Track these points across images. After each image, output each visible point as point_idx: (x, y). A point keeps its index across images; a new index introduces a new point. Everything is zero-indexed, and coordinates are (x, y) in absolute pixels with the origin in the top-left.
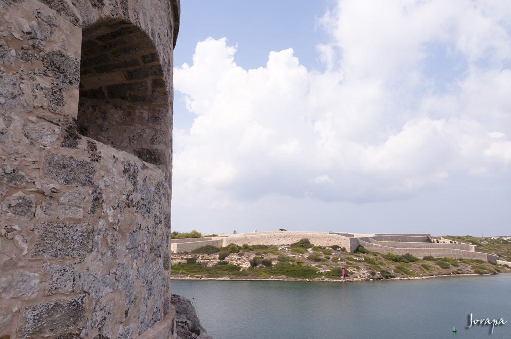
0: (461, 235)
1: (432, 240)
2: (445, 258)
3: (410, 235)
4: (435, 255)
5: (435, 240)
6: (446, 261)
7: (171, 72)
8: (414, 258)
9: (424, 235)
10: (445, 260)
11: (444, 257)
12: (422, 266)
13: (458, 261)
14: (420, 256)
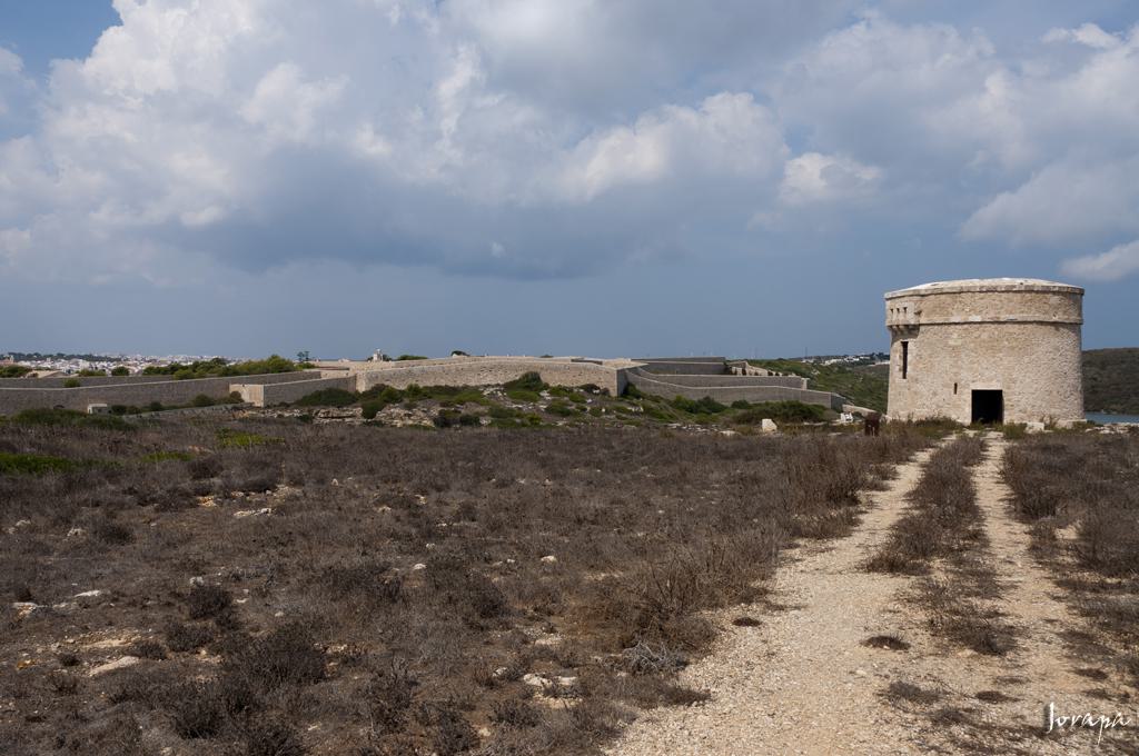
1: (734, 369)
5: (740, 370)
9: (714, 360)
14: (727, 402)
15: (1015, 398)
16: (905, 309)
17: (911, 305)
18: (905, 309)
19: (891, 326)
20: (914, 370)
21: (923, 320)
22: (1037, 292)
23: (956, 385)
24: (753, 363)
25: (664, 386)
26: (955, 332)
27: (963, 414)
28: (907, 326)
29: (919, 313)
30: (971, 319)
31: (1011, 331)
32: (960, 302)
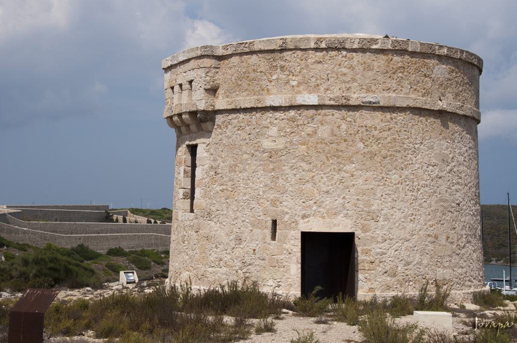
0: (154, 208)
1: (115, 217)
2: (143, 251)
3: (73, 207)
4: (126, 246)
5: (120, 218)
6: (145, 256)
7: (481, 62)
8: (92, 252)
9: (98, 208)
10: (143, 253)
11: (140, 249)
12: (106, 266)
13: (163, 256)
14: (102, 249)
15: (376, 248)
16: (191, 82)
17: (198, 74)
18: (191, 82)
19: (171, 118)
20: (205, 196)
21: (221, 103)
22: (413, 54)
23: (274, 223)
24: (135, 211)
25: (34, 234)
26: (274, 124)
27: (285, 279)
28: (193, 114)
29: (213, 91)
30: (300, 100)
31: (369, 123)
32: (282, 67)
